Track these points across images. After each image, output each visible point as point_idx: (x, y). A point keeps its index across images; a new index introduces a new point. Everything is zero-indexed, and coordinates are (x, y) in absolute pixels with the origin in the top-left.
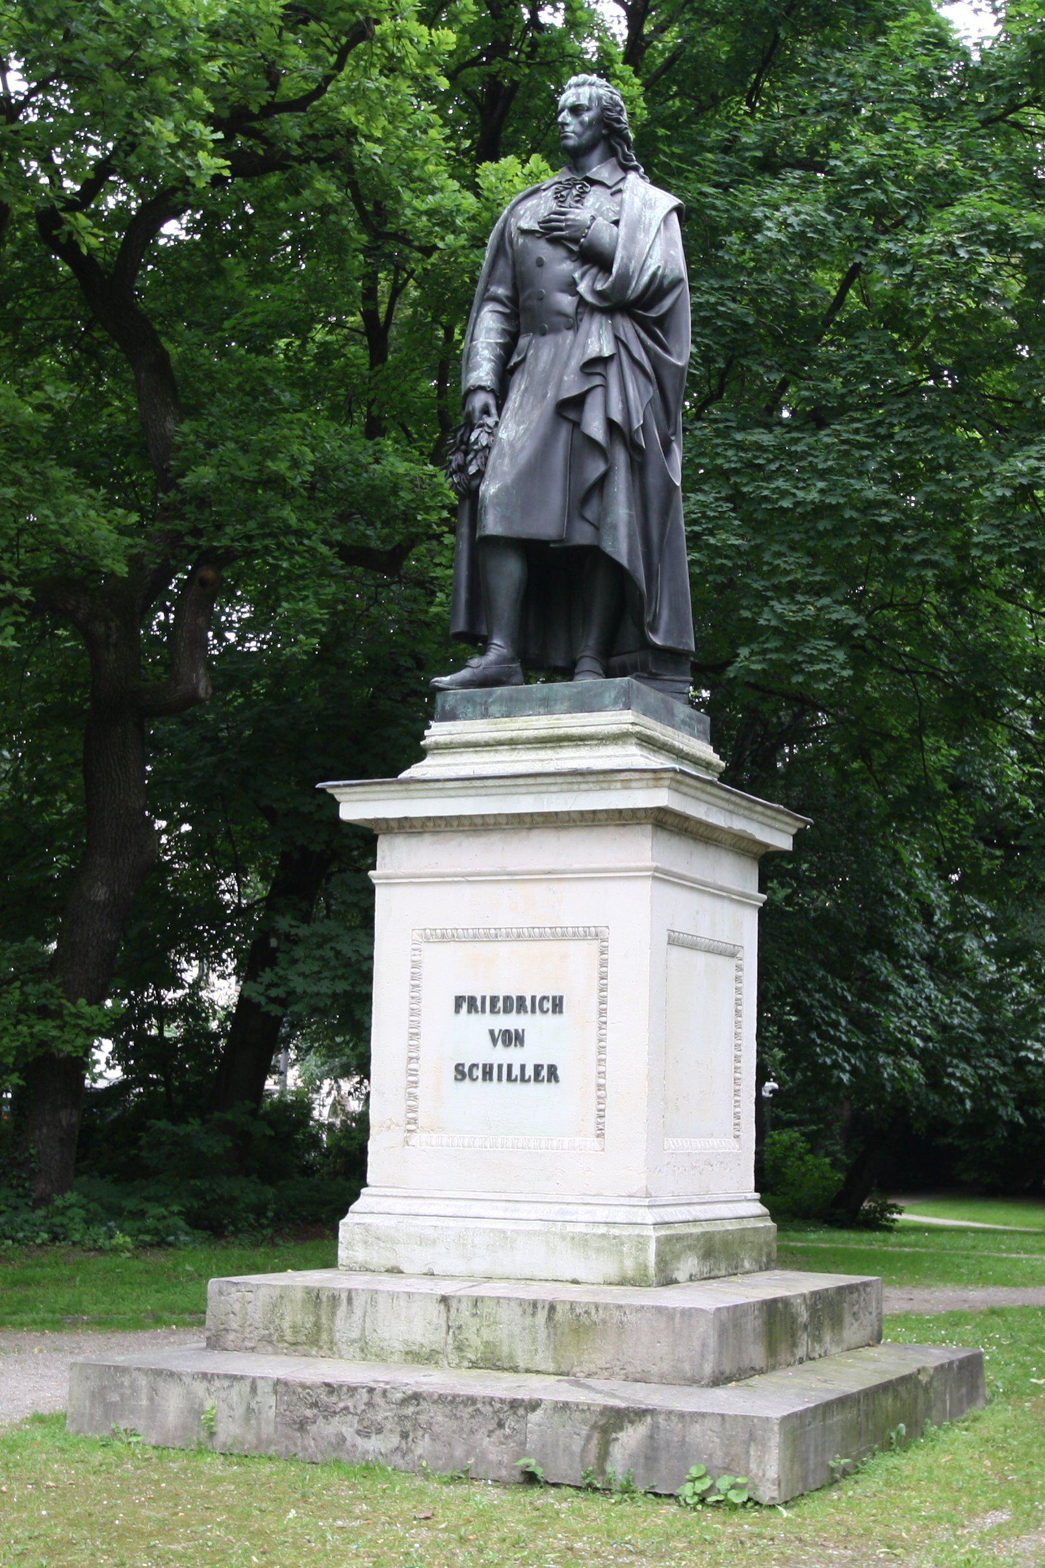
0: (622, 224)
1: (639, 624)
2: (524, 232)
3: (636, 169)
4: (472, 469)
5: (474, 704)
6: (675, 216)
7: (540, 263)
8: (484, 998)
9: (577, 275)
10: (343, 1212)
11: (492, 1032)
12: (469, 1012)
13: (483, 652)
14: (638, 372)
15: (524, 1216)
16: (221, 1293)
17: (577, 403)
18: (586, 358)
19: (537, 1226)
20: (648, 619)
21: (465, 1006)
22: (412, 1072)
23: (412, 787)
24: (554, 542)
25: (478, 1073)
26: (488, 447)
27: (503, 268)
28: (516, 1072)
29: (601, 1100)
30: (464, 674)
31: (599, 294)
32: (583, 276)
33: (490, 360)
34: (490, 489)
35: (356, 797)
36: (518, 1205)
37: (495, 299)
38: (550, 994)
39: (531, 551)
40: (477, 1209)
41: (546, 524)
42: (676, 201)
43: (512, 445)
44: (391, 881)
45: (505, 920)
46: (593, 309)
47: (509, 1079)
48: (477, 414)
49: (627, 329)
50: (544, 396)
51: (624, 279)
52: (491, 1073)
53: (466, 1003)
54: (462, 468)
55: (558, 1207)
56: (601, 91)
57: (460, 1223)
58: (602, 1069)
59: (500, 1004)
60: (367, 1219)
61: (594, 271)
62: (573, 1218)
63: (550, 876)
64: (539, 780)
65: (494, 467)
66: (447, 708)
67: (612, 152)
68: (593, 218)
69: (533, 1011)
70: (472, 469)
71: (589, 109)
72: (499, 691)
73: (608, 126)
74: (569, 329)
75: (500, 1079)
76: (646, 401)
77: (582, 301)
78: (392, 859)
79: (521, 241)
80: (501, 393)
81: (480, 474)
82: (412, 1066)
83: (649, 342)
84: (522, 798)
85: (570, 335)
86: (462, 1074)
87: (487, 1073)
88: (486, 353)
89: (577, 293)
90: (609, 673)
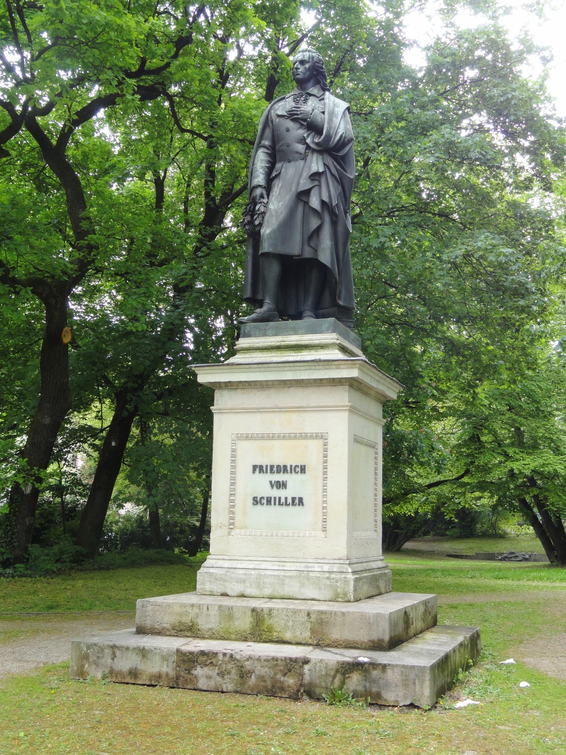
0: (326, 113)
2: (279, 116)
4: (257, 222)
7: (288, 130)
8: (267, 466)
9: (305, 135)
10: (199, 567)
11: (271, 482)
12: (260, 472)
13: (261, 306)
15: (288, 569)
16: (143, 606)
17: (307, 193)
18: (312, 172)
19: (294, 573)
21: (258, 470)
22: (232, 501)
23: (234, 367)
25: (265, 501)
26: (264, 213)
27: (268, 132)
28: (283, 500)
29: (325, 514)
30: (254, 316)
31: (317, 144)
32: (308, 136)
34: (266, 231)
35: (205, 372)
36: (285, 564)
37: (264, 147)
38: (299, 464)
39: (285, 260)
40: (264, 565)
41: (295, 247)
43: (276, 211)
44: (221, 411)
45: (277, 430)
46: (314, 151)
47: (280, 504)
48: (258, 197)
49: (330, 161)
51: (328, 137)
52: (270, 501)
53: (258, 469)
55: (304, 565)
56: (314, 54)
57: (257, 572)
58: (325, 499)
59: (275, 469)
60: (211, 570)
61: (313, 134)
62: (312, 569)
63: (300, 409)
64: (264, 365)
65: (268, 221)
66: (246, 331)
67: (317, 82)
68: (313, 110)
69: (291, 472)
70: (257, 222)
71: (308, 62)
72: (271, 324)
73: (316, 70)
75: (275, 504)
77: (308, 147)
78: (222, 401)
80: (268, 188)
81: (261, 225)
82: (232, 498)
83: (338, 167)
84: (287, 373)
86: (256, 501)
87: (269, 501)
88: (261, 170)
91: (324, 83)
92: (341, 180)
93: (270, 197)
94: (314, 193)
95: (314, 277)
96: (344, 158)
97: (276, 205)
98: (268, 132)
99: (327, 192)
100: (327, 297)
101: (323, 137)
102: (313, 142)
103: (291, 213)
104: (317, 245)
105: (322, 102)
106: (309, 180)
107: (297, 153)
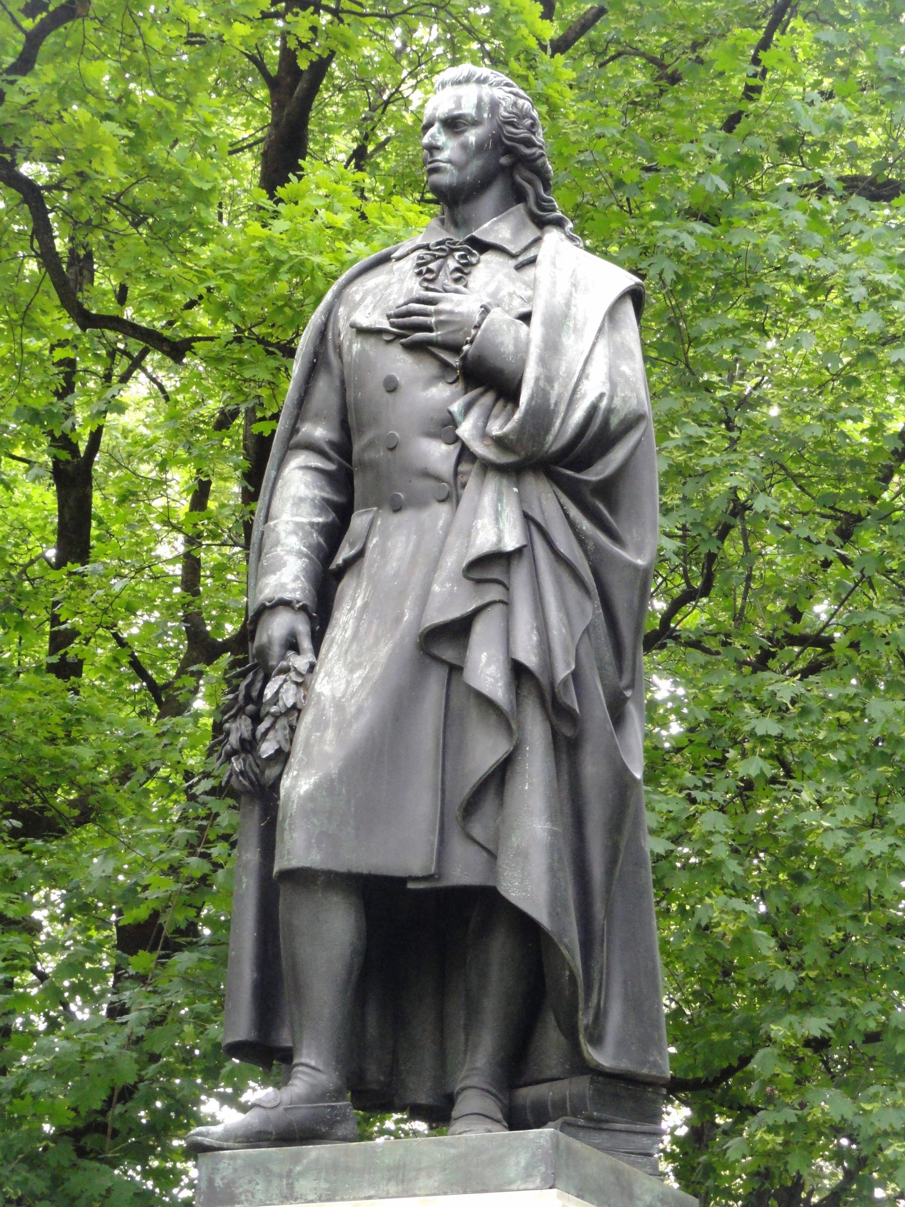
0: (536, 320)
1: (570, 1031)
3: (559, 223)
4: (267, 749)
5: (268, 1175)
6: (629, 308)
7: (392, 387)
9: (456, 408)
14: (566, 578)
17: (459, 630)
18: (474, 553)
20: (584, 1019)
24: (416, 879)
26: (296, 710)
27: (324, 391)
31: (500, 442)
32: (468, 408)
33: (300, 554)
34: (298, 784)
37: (311, 447)
39: (380, 899)
41: (406, 849)
42: (631, 280)
43: (339, 707)
46: (487, 467)
48: (276, 650)
49: (547, 501)
50: (398, 619)
51: (541, 416)
54: (249, 746)
56: (499, 93)
61: (488, 399)
65: (307, 745)
68: (486, 310)
70: (267, 749)
71: (475, 123)
72: (314, 1151)
73: (509, 151)
74: (442, 501)
76: (580, 628)
77: (465, 454)
79: (356, 347)
81: (282, 757)
83: (585, 525)
85: (443, 511)
89: (457, 439)
90: (516, 1119)
91: (539, 200)
92: (599, 582)
93: (323, 650)
94: (484, 633)
95: (498, 962)
96: (608, 490)
97: (342, 681)
98: (324, 391)
99: (541, 625)
100: (551, 1042)
101: (517, 416)
102: (484, 435)
103: (397, 711)
104: (497, 837)
105: (530, 272)
106: (468, 584)
107: (427, 474)
